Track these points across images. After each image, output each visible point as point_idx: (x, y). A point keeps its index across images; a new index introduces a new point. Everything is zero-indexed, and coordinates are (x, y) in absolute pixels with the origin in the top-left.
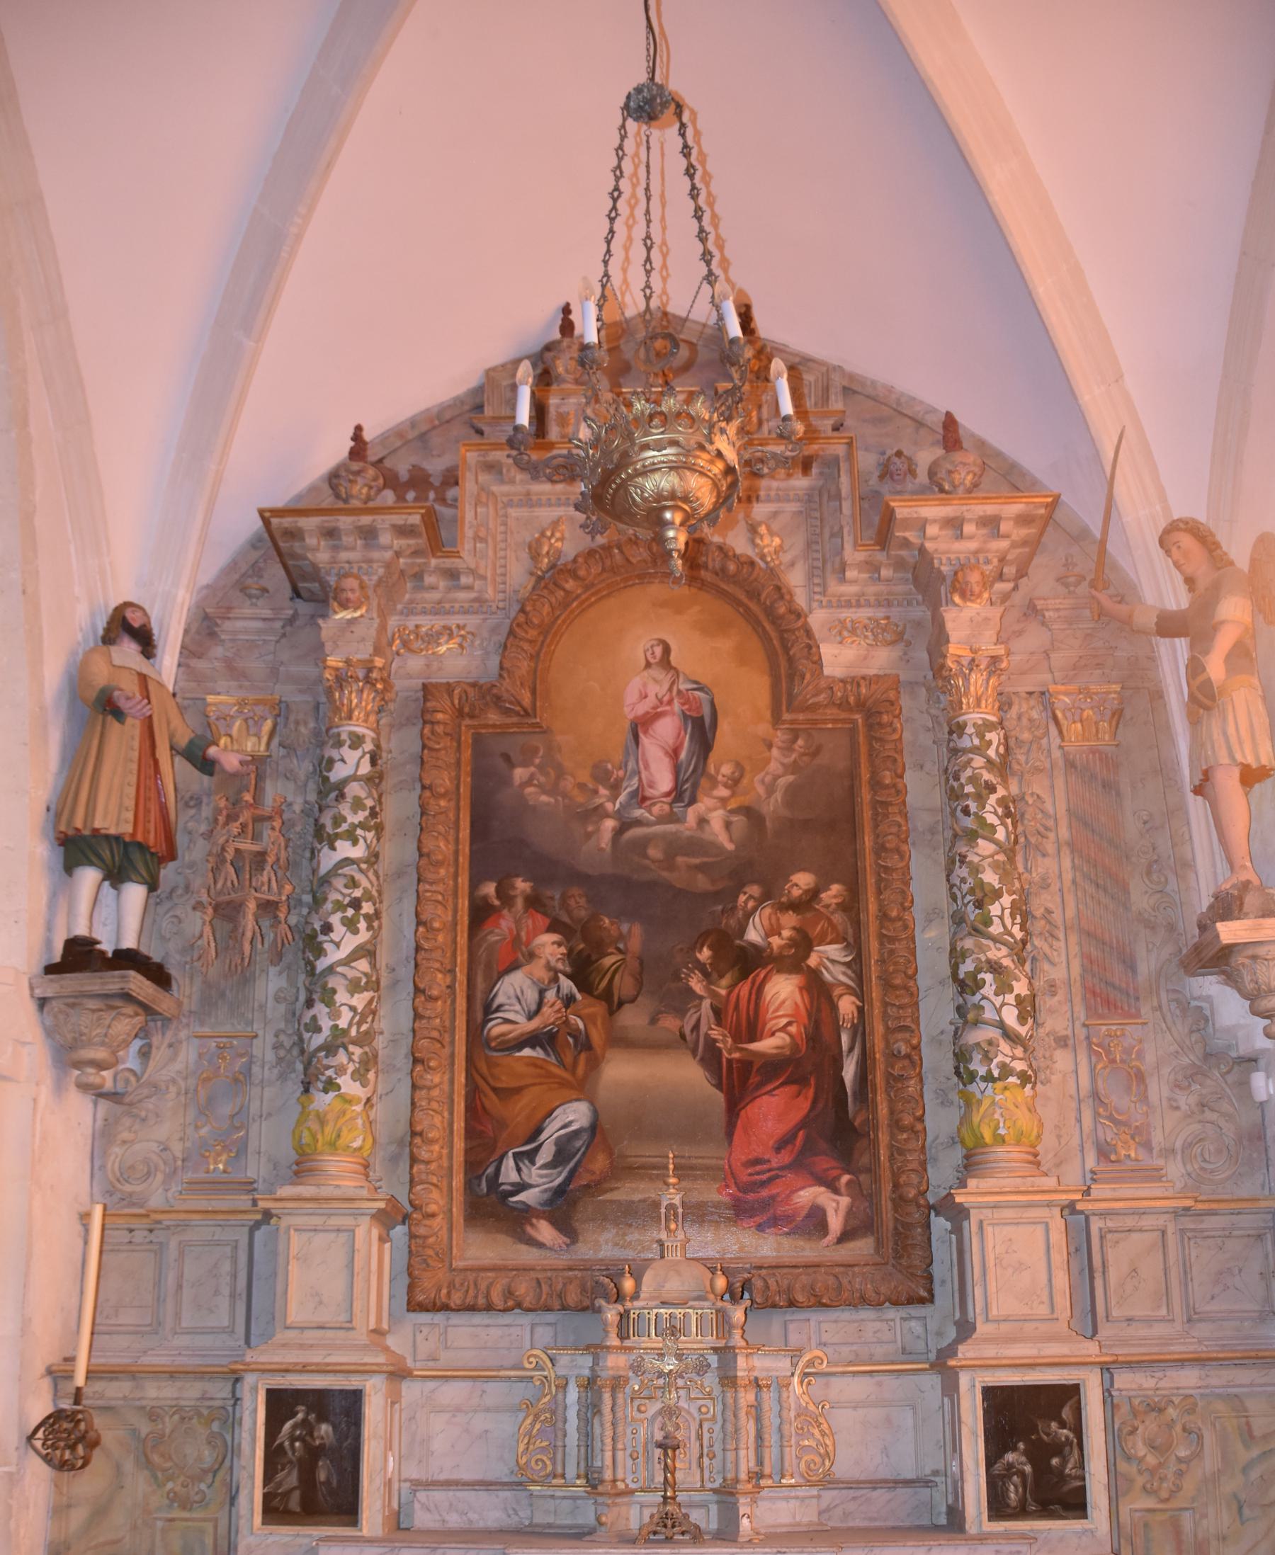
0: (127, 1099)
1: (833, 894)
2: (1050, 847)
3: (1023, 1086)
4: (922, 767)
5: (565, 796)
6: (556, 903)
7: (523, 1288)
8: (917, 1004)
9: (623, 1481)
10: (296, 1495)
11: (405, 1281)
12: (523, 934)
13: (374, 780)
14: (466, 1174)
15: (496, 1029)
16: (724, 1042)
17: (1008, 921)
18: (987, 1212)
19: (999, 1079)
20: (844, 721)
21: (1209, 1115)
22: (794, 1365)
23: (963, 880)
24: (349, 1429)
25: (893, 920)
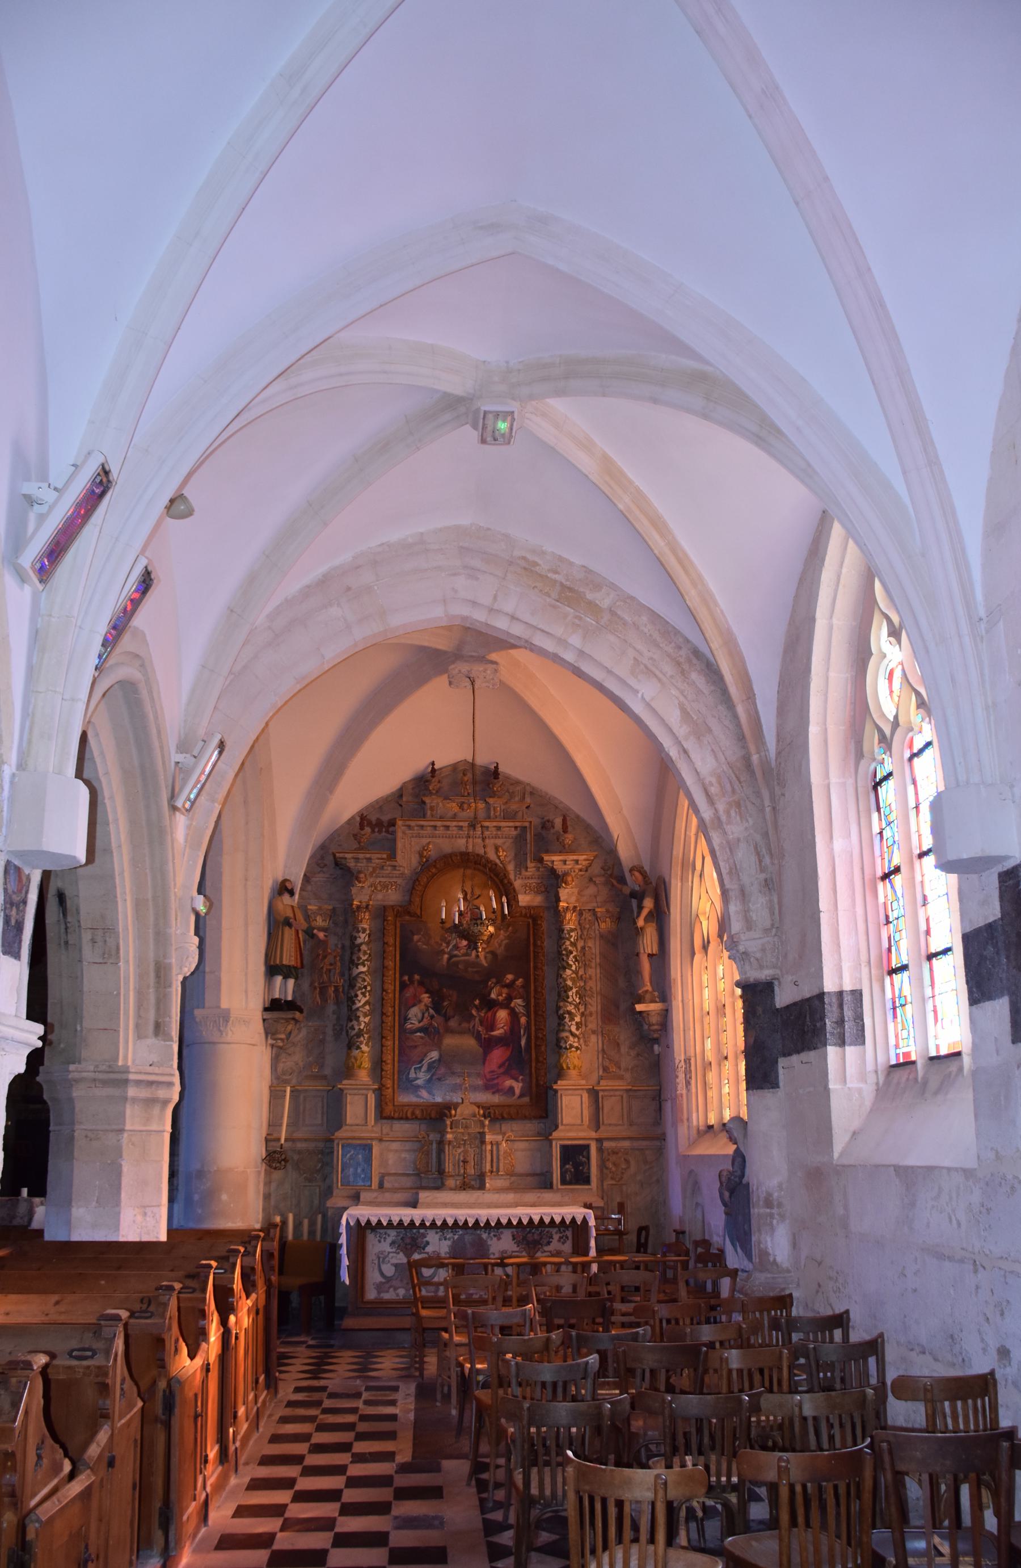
1: (520, 982)
2: (593, 965)
7: (418, 1112)
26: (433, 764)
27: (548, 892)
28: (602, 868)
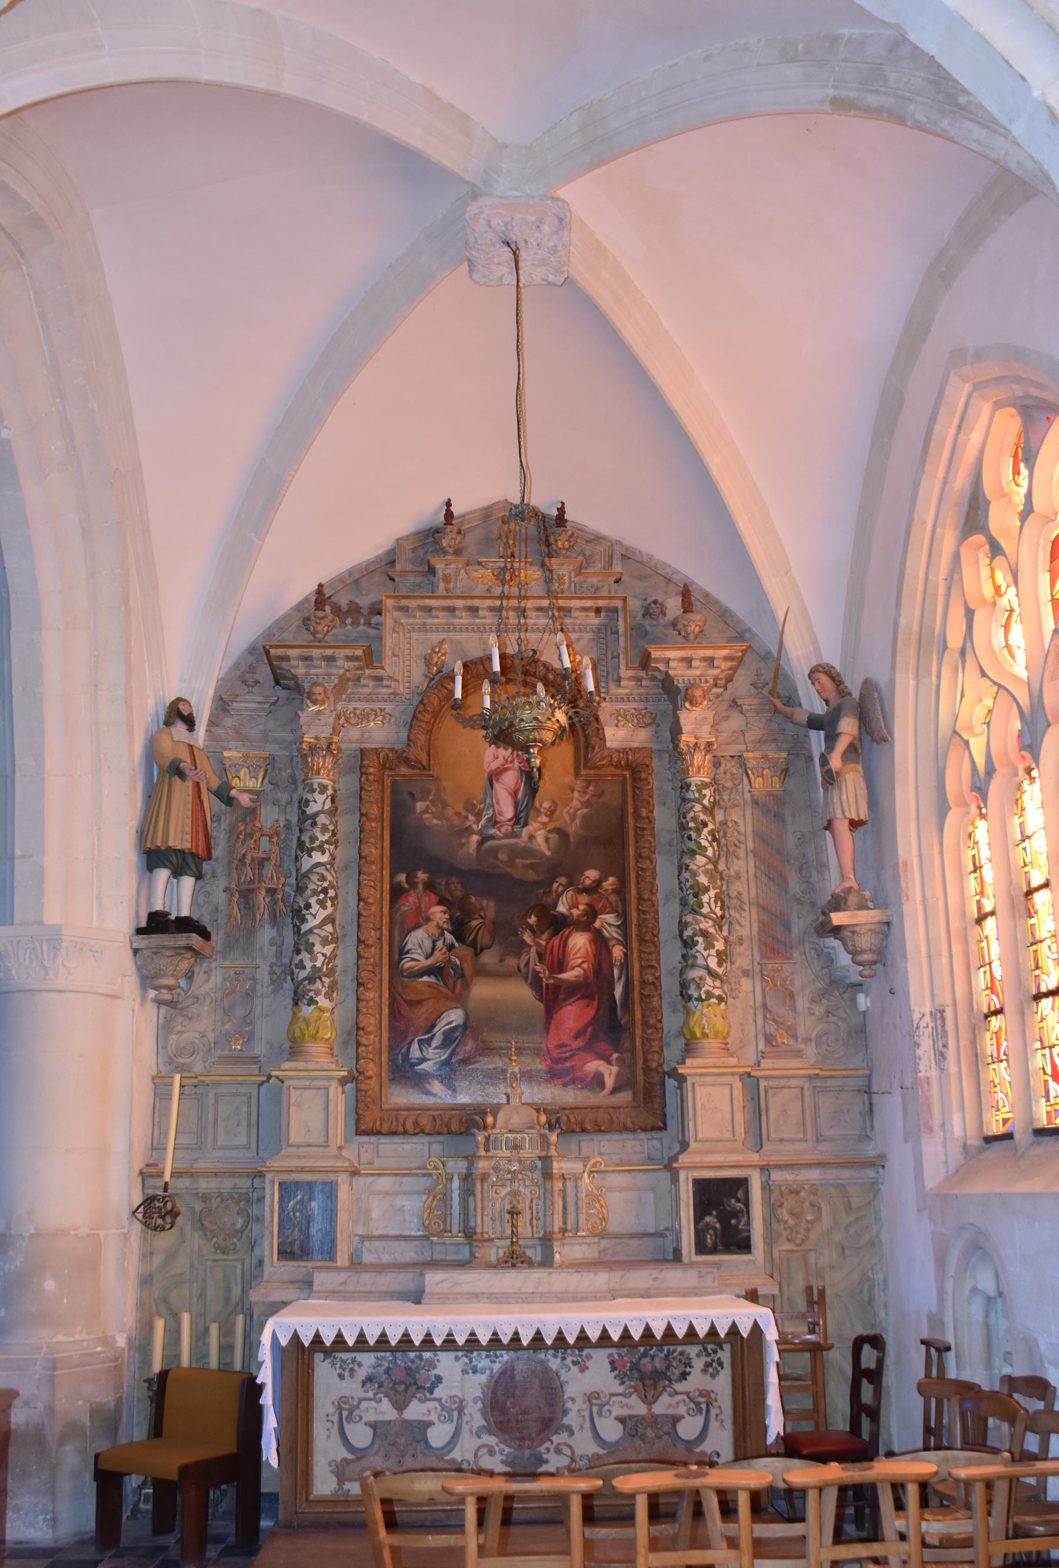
0: (180, 1006)
1: (610, 882)
2: (742, 853)
3: (719, 1004)
4: (665, 804)
5: (448, 820)
6: (443, 887)
7: (424, 1121)
11: (354, 1117)
12: (423, 906)
13: (332, 813)
15: (407, 964)
17: (713, 905)
18: (697, 1078)
20: (618, 775)
21: (832, 1018)
22: (585, 1166)
23: (687, 880)
25: (645, 900)
26: (449, 504)
27: (658, 726)
28: (753, 685)
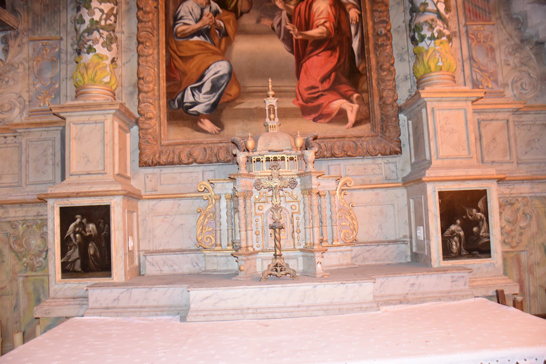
7: (198, 153)
8: (388, 11)
9: (252, 247)
10: (78, 262)
14: (167, 98)
16: (294, 31)
19: (438, 38)
24: (104, 226)
